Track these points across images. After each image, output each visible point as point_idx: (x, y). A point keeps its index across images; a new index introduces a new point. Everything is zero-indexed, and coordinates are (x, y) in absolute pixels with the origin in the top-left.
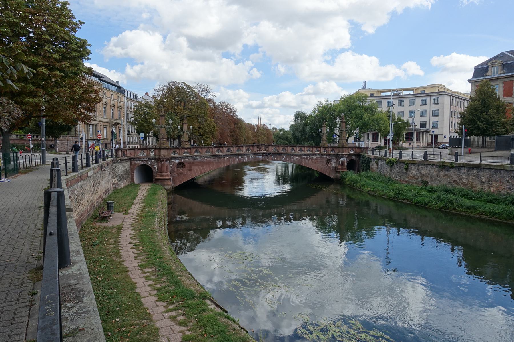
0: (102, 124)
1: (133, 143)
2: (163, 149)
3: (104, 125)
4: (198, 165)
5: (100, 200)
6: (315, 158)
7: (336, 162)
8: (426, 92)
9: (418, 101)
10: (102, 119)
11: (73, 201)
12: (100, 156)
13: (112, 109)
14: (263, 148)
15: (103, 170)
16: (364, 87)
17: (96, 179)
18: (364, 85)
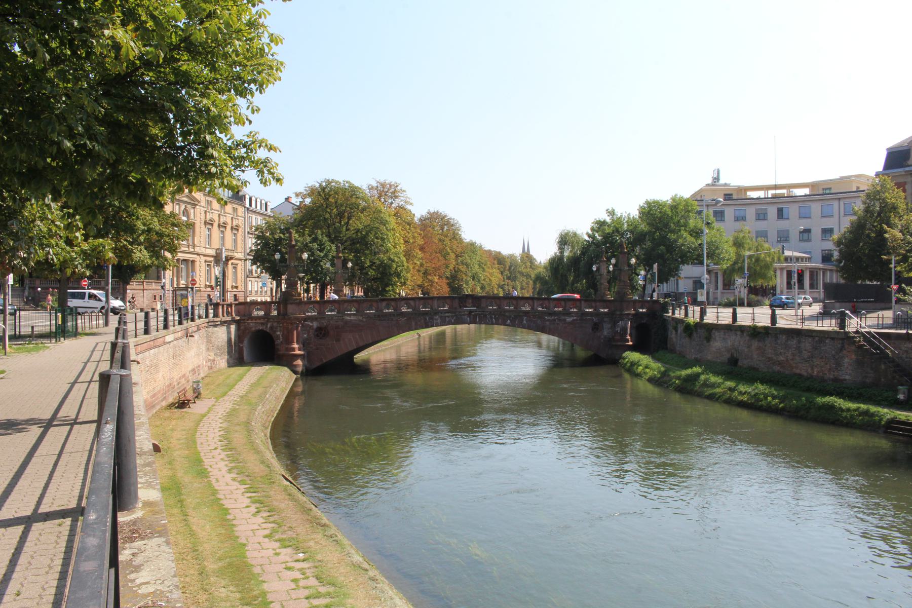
0: (203, 258)
1: (259, 293)
2: (292, 304)
3: (206, 261)
5: (183, 381)
6: (569, 319)
8: (832, 191)
9: (816, 208)
10: (203, 251)
11: (143, 373)
12: (187, 314)
13: (222, 231)
14: (470, 301)
15: (190, 336)
16: (716, 179)
17: (177, 349)
18: (715, 176)
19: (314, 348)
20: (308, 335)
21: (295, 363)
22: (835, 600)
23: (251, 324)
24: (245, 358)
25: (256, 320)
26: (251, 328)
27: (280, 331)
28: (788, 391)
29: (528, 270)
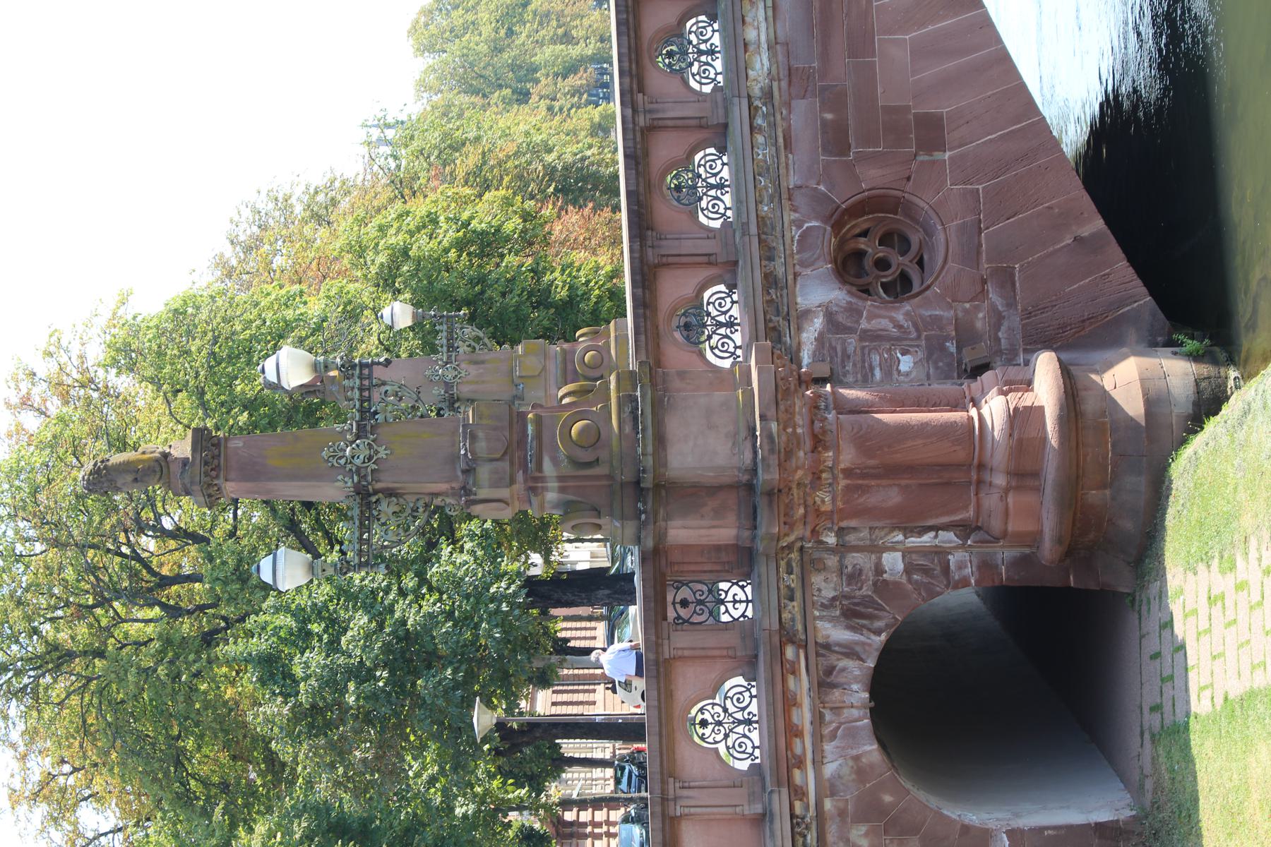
2: (660, 441)
4: (861, 44)
19: (994, 296)
20: (900, 341)
21: (1133, 406)
22: (1139, 739)
23: (829, 769)
24: (1103, 816)
25: (794, 732)
26: (861, 773)
27: (877, 549)
28: (854, 300)
29: (484, 16)
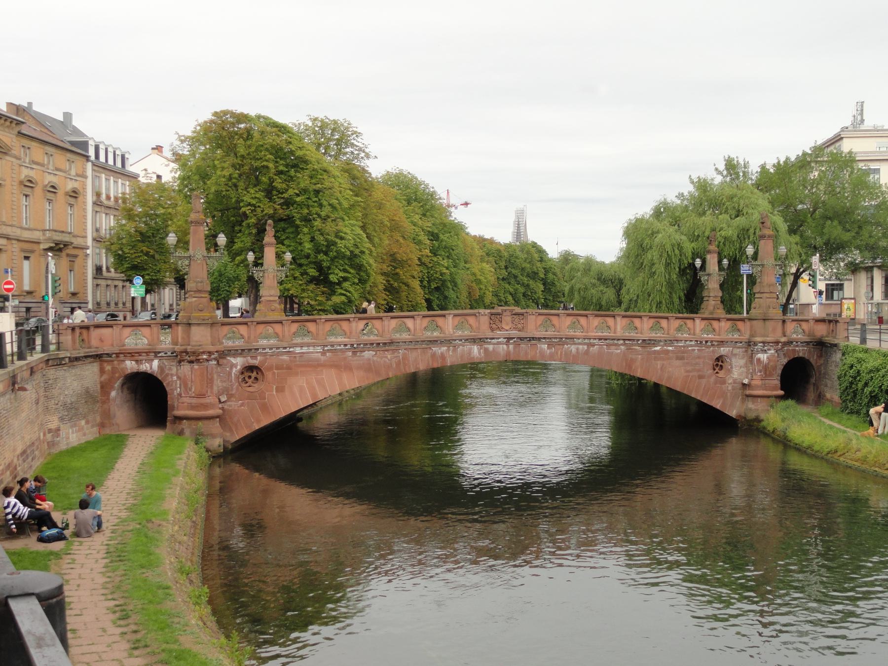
0: (16, 246)
7: (746, 366)
